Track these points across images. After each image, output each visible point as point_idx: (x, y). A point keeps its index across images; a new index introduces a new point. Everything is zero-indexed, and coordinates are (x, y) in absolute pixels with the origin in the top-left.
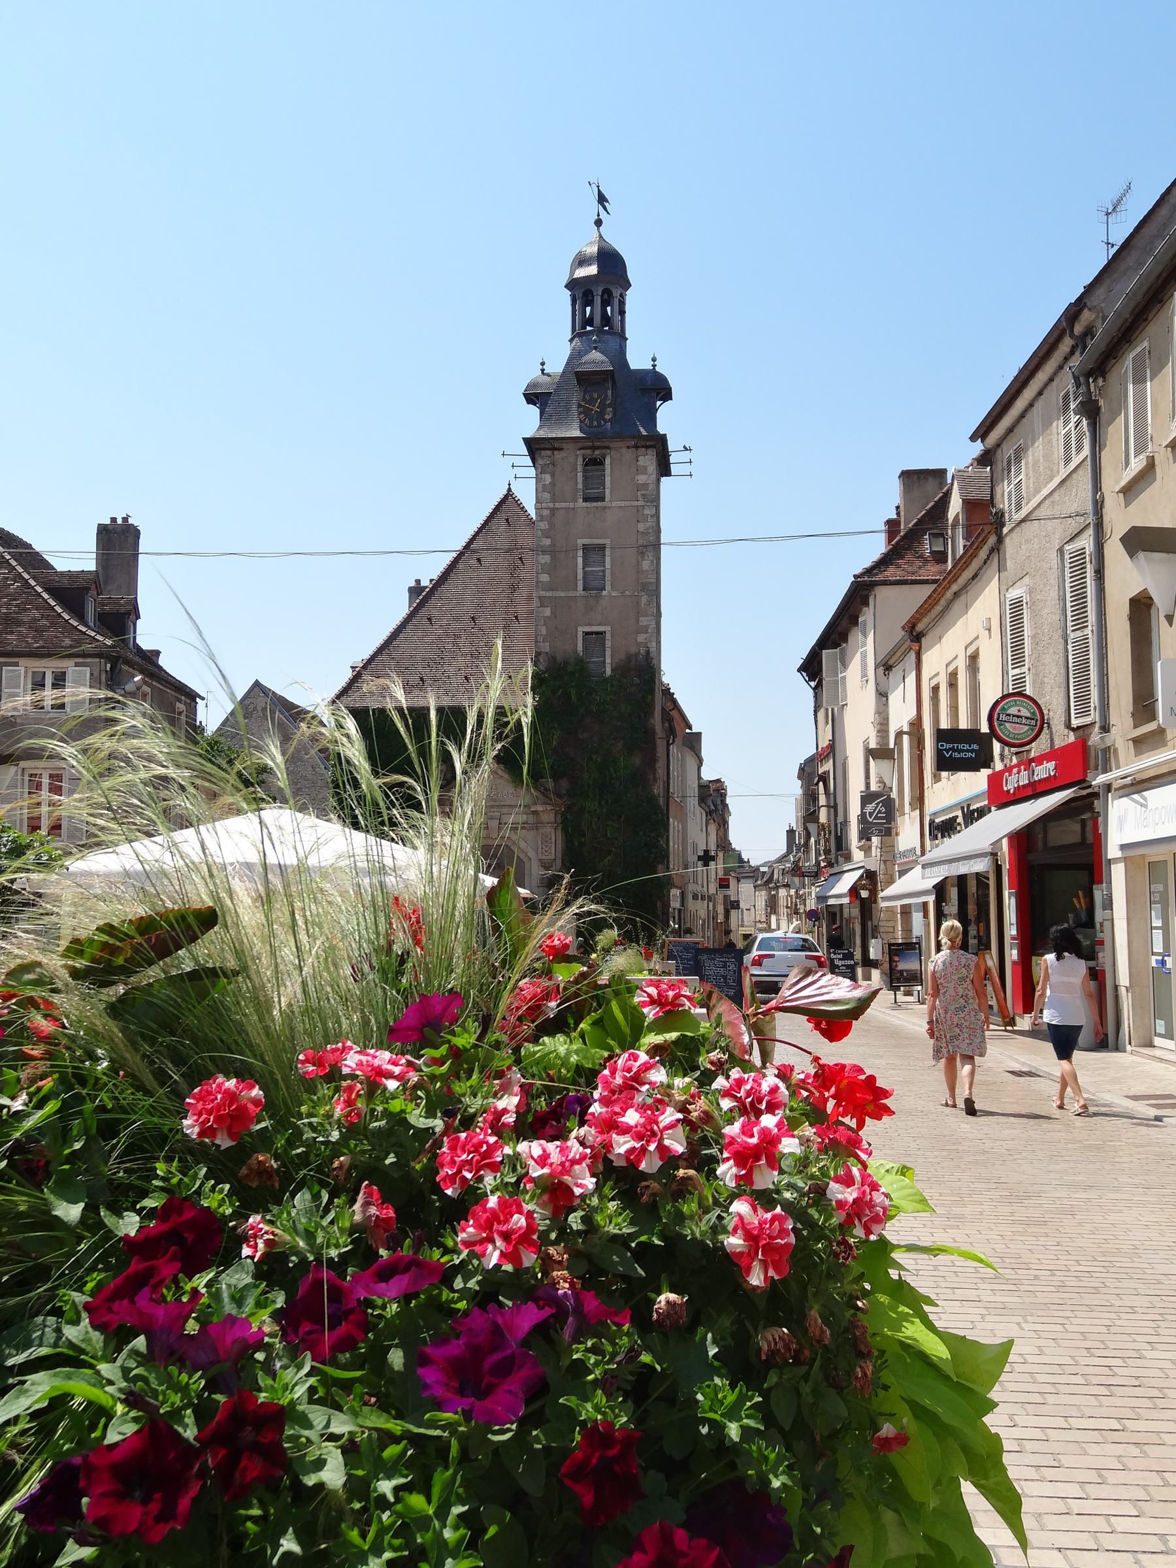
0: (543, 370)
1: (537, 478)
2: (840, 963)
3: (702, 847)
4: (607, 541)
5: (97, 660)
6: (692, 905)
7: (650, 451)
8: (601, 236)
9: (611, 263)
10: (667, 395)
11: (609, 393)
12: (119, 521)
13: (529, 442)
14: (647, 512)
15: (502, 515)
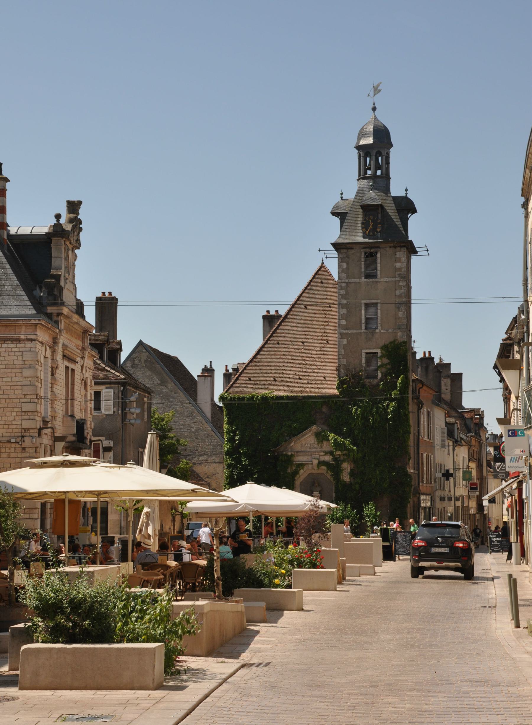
0: (342, 198)
2: (494, 540)
4: (379, 301)
5: (117, 386)
6: (439, 505)
7: (402, 249)
8: (375, 117)
9: (382, 136)
10: (414, 211)
11: (380, 215)
12: (107, 294)
13: (334, 245)
14: (401, 284)
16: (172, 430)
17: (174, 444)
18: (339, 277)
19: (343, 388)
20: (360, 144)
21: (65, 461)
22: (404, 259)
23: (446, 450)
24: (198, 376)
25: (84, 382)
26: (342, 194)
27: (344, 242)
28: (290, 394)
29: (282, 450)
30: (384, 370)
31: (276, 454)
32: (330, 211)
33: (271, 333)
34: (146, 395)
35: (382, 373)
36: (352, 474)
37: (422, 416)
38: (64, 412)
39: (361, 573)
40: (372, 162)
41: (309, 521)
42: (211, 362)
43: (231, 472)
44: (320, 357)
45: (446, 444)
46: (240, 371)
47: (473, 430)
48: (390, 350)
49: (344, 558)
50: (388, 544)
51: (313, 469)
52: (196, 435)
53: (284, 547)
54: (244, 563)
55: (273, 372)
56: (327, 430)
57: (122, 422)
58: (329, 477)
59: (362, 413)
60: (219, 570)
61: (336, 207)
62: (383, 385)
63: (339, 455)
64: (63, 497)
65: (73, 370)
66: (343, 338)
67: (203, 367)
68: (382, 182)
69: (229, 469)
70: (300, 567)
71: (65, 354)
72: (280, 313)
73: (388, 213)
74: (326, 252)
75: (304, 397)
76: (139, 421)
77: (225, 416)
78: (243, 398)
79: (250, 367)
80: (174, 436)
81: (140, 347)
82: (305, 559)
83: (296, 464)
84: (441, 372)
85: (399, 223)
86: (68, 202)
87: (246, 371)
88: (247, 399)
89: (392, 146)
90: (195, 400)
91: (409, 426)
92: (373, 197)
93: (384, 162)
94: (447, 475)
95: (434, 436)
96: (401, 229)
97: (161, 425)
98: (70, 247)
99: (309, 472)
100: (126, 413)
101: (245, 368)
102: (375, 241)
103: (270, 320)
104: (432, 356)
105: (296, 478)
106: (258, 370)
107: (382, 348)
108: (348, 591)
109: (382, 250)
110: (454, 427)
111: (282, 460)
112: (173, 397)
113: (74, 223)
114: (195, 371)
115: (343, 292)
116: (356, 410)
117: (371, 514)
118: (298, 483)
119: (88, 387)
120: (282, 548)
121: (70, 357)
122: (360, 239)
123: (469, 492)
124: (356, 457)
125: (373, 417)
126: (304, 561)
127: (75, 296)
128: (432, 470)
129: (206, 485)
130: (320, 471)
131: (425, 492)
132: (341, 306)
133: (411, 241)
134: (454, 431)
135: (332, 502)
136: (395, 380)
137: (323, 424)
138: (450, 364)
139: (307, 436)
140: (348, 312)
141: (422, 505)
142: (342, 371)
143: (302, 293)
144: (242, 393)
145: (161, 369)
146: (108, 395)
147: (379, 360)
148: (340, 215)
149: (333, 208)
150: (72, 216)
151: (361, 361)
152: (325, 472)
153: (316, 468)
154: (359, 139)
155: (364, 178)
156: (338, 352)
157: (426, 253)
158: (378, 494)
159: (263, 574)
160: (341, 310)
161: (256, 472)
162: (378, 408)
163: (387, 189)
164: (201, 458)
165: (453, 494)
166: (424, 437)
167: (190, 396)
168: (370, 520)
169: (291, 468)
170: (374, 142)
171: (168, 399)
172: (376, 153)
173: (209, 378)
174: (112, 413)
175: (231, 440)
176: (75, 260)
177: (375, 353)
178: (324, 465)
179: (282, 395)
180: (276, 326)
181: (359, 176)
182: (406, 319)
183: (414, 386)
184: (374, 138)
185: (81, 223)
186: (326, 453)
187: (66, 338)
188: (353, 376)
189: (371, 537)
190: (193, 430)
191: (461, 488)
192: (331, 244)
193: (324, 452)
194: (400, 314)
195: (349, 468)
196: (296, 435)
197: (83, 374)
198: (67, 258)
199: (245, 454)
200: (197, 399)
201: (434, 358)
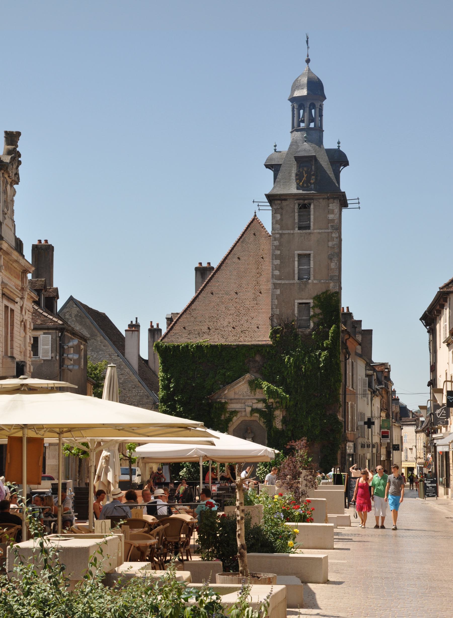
0: (275, 150)
2: (429, 485)
3: (368, 415)
4: (312, 252)
5: (54, 331)
6: (360, 451)
7: (335, 201)
8: (309, 70)
9: (316, 87)
10: (346, 163)
11: (313, 167)
13: (268, 196)
14: (334, 235)
18: (273, 228)
21: (22, 385)
22: (336, 211)
24: (126, 331)
25: (23, 323)
26: (275, 146)
27: (279, 193)
29: (216, 398)
30: (316, 320)
31: (210, 401)
33: (203, 285)
36: (284, 421)
38: (4, 353)
40: (306, 114)
42: (137, 318)
44: (253, 307)
46: (175, 320)
47: (383, 383)
48: (322, 300)
51: (246, 416)
56: (260, 379)
57: (60, 368)
58: (262, 424)
59: (295, 362)
60: (243, 535)
61: (269, 159)
62: (315, 335)
63: (272, 402)
64: (19, 434)
65: (12, 311)
67: (130, 323)
68: (315, 134)
71: (4, 292)
72: (212, 265)
73: (321, 165)
74: (260, 204)
75: (238, 346)
76: (76, 367)
78: (178, 346)
79: (184, 316)
81: (70, 302)
84: (356, 327)
85: (332, 175)
86: (6, 132)
87: (180, 320)
89: (326, 98)
90: (123, 354)
91: (340, 374)
92: (307, 149)
93: (318, 114)
95: (357, 386)
96: (335, 180)
98: (9, 181)
99: (242, 419)
100: (64, 358)
101: (179, 318)
102: (309, 192)
103: (202, 272)
104: (350, 311)
106: (192, 319)
107: (314, 298)
108: (349, 549)
109: (315, 202)
110: (372, 378)
111: (215, 407)
113: (13, 155)
114: (122, 327)
115: (276, 243)
116: (289, 359)
119: (28, 330)
121: (9, 296)
122: (293, 190)
123: (380, 440)
125: (305, 366)
127: (14, 234)
130: (252, 418)
132: (275, 257)
136: (327, 330)
137: (257, 372)
138: (360, 321)
139: (240, 384)
140: (281, 262)
142: (275, 320)
143: (236, 244)
145: (91, 324)
146: (46, 342)
148: (273, 167)
150: (11, 147)
152: (257, 419)
153: (249, 415)
154: (293, 91)
155: (297, 130)
156: (272, 302)
157: (357, 206)
160: (275, 261)
162: (310, 357)
163: (320, 142)
165: (371, 442)
166: (349, 387)
169: (225, 415)
170: (308, 93)
171: (98, 352)
172: (310, 105)
173: (136, 333)
174: (50, 358)
176: (14, 195)
177: (308, 303)
178: (257, 413)
179: (216, 344)
181: (292, 129)
184: (308, 90)
185: (19, 156)
186: (259, 401)
187: (5, 276)
188: (286, 325)
193: (257, 399)
195: (281, 415)
196: (231, 383)
197: (23, 315)
198: (5, 192)
199: (180, 401)
200: (124, 353)
201: (352, 313)
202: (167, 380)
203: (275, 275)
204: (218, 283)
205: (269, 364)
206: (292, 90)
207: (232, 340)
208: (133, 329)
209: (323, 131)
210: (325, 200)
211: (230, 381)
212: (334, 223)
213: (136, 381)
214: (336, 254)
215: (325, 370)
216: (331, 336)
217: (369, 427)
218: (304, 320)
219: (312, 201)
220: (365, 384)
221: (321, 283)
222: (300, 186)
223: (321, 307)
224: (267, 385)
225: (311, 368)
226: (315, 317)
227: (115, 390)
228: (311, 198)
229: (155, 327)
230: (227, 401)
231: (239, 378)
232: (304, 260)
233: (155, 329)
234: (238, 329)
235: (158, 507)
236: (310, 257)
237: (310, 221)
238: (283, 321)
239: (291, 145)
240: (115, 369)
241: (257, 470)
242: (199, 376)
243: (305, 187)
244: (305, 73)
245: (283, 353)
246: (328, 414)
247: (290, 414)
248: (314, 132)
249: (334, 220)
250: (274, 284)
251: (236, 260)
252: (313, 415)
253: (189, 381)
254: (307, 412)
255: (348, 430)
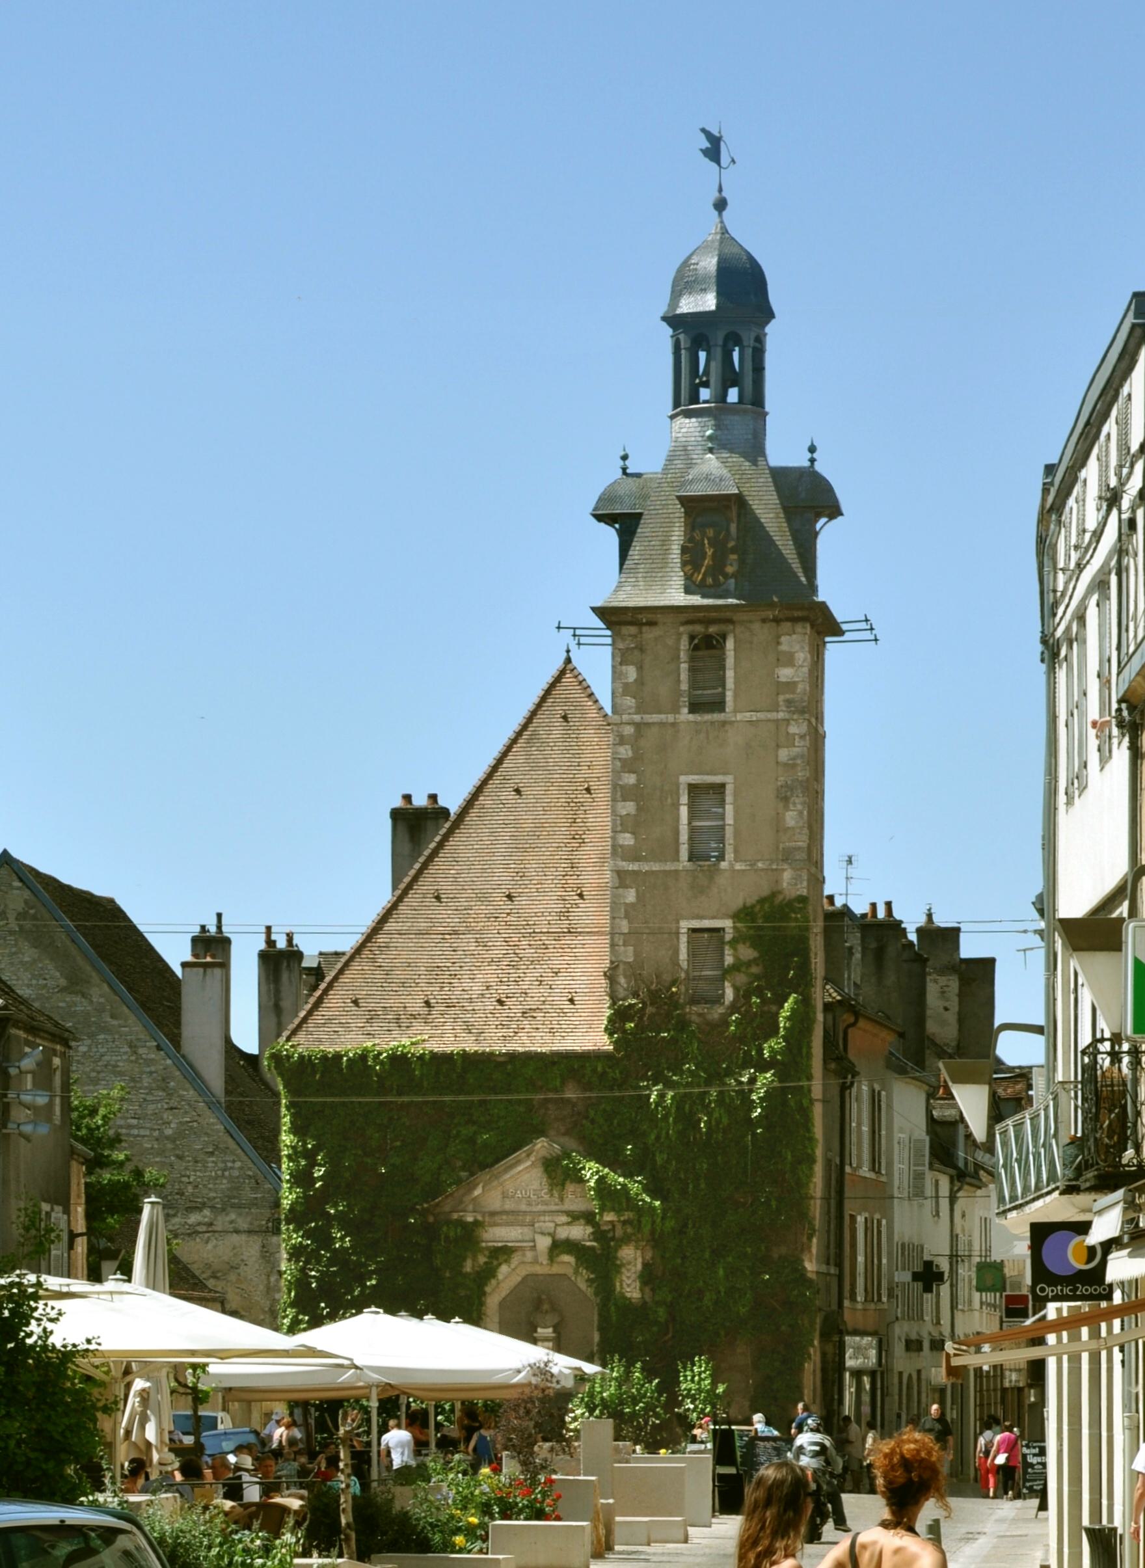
1: (613, 644)
4: (728, 779)
6: (902, 1362)
7: (799, 628)
8: (724, 231)
10: (834, 511)
11: (733, 527)
13: (602, 612)
14: (793, 729)
15: (555, 708)
16: (120, 1141)
17: (126, 1186)
19: (624, 1031)
20: (679, 311)
22: (803, 656)
23: (929, 1204)
24: (184, 965)
26: (625, 458)
27: (631, 604)
28: (471, 1047)
29: (447, 1209)
30: (741, 979)
31: (431, 1219)
32: (590, 510)
33: (417, 866)
34: (58, 1047)
35: (736, 989)
36: (648, 1277)
37: (855, 1105)
39: (652, 1538)
40: (713, 364)
41: (528, 1412)
42: (219, 916)
43: (303, 1270)
45: (929, 1191)
46: (328, 979)
49: (611, 1501)
50: (732, 1470)
51: (536, 1261)
52: (176, 1148)
53: (470, 1471)
54: (391, 1501)
55: (422, 982)
56: (578, 1152)
59: (679, 1101)
60: (350, 1510)
61: (607, 498)
63: (611, 1222)
66: (627, 887)
69: (297, 1261)
70: (505, 1516)
72: (442, 802)
73: (757, 520)
74: (578, 632)
75: (512, 1057)
76: (43, 1130)
77: (283, 1110)
78: (338, 1057)
79: (355, 966)
80: (128, 1159)
82: (518, 1500)
83: (487, 1248)
84: (927, 960)
85: (788, 550)
87: (343, 979)
88: (349, 1060)
90: (176, 1040)
91: (811, 1139)
92: (714, 472)
94: (929, 1276)
95: (890, 1164)
97: (89, 1129)
99: (523, 1271)
100: (8, 1103)
101: (347, 965)
104: (897, 915)
105: (488, 1289)
106: (379, 974)
107: (736, 917)
109: (739, 629)
112: (105, 1029)
114: (175, 952)
115: (625, 752)
116: (662, 1096)
117: (700, 1391)
118: (493, 1301)
120: (465, 1473)
122: (676, 596)
123: (1002, 1322)
124: (658, 1229)
125: (709, 1114)
126: (517, 1504)
128: (884, 1261)
129: (214, 1300)
130: (556, 1269)
131: (860, 1327)
132: (620, 793)
133: (824, 603)
134: (954, 1144)
135: (589, 1359)
136: (774, 1008)
138: (956, 931)
139: (520, 1168)
140: (639, 809)
141: (850, 1363)
142: (622, 980)
144: (332, 1042)
145: (68, 942)
147: (728, 951)
148: (625, 523)
149: (600, 499)
151: (677, 951)
152: (570, 1271)
153: (544, 1259)
155: (688, 414)
156: (612, 924)
157: (868, 635)
158: (722, 1333)
159: (431, 1524)
160: (620, 804)
161: (373, 1272)
163: (755, 449)
164: (193, 1218)
166: (859, 1167)
167: (159, 1025)
168: (696, 1407)
169: (474, 1259)
172: (727, 339)
173: (218, 971)
175: (302, 1178)
178: (569, 1253)
179: (448, 1050)
180: (432, 845)
182: (806, 831)
183: (830, 1022)
184: (720, 295)
186: (574, 1217)
188: (654, 996)
189: (690, 1453)
190: (168, 1132)
191: (977, 1314)
192: (594, 609)
193: (568, 1213)
194: (791, 818)
195: (640, 1260)
199: (343, 1221)
200: (179, 1035)
202: (304, 1158)
203: (621, 846)
204: (462, 860)
205: (605, 1111)
206: (673, 292)
207: (496, 1042)
208: (209, 959)
209: (767, 414)
210: (768, 625)
211: (489, 1160)
212: (793, 692)
213: (218, 1131)
214: (808, 784)
215: (767, 1129)
216: (785, 1028)
217: (928, 1289)
218: (707, 979)
219: (731, 627)
220: (919, 1153)
221: (756, 870)
222: (694, 583)
223: (755, 940)
224: (597, 1172)
225: (725, 1121)
226: (739, 971)
227: (160, 1251)
228: (723, 617)
229: (281, 944)
230: (480, 1218)
231: (515, 1151)
232: (706, 803)
233: (281, 952)
234: (515, 1007)
235: (245, 1486)
236: (724, 793)
237: (724, 686)
238: (644, 982)
239: (670, 459)
240: (160, 1207)
241: (568, 1419)
242: (398, 1143)
243: (710, 586)
244: (713, 241)
245: (645, 1078)
246: (776, 1256)
247: (663, 1257)
248: (736, 418)
249: (795, 684)
250: (620, 874)
251: (508, 795)
252: (730, 1259)
253: (369, 1160)
254: (713, 1252)
255: (853, 1298)
